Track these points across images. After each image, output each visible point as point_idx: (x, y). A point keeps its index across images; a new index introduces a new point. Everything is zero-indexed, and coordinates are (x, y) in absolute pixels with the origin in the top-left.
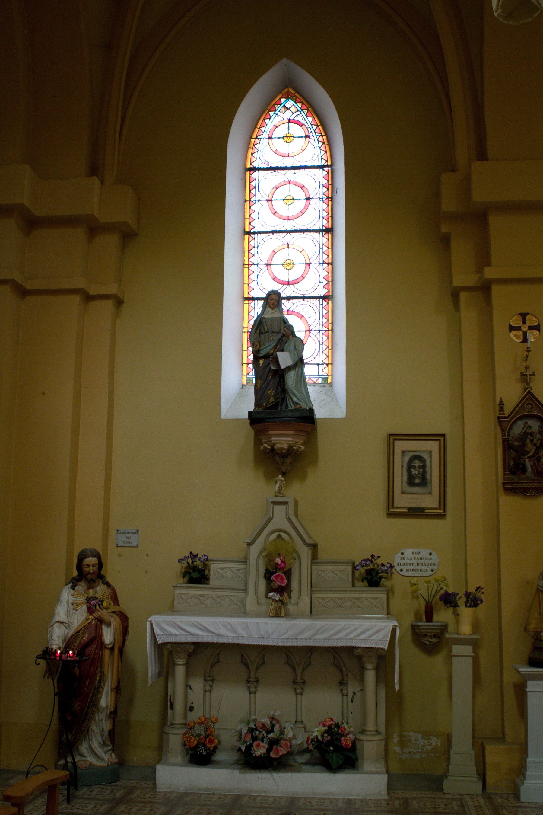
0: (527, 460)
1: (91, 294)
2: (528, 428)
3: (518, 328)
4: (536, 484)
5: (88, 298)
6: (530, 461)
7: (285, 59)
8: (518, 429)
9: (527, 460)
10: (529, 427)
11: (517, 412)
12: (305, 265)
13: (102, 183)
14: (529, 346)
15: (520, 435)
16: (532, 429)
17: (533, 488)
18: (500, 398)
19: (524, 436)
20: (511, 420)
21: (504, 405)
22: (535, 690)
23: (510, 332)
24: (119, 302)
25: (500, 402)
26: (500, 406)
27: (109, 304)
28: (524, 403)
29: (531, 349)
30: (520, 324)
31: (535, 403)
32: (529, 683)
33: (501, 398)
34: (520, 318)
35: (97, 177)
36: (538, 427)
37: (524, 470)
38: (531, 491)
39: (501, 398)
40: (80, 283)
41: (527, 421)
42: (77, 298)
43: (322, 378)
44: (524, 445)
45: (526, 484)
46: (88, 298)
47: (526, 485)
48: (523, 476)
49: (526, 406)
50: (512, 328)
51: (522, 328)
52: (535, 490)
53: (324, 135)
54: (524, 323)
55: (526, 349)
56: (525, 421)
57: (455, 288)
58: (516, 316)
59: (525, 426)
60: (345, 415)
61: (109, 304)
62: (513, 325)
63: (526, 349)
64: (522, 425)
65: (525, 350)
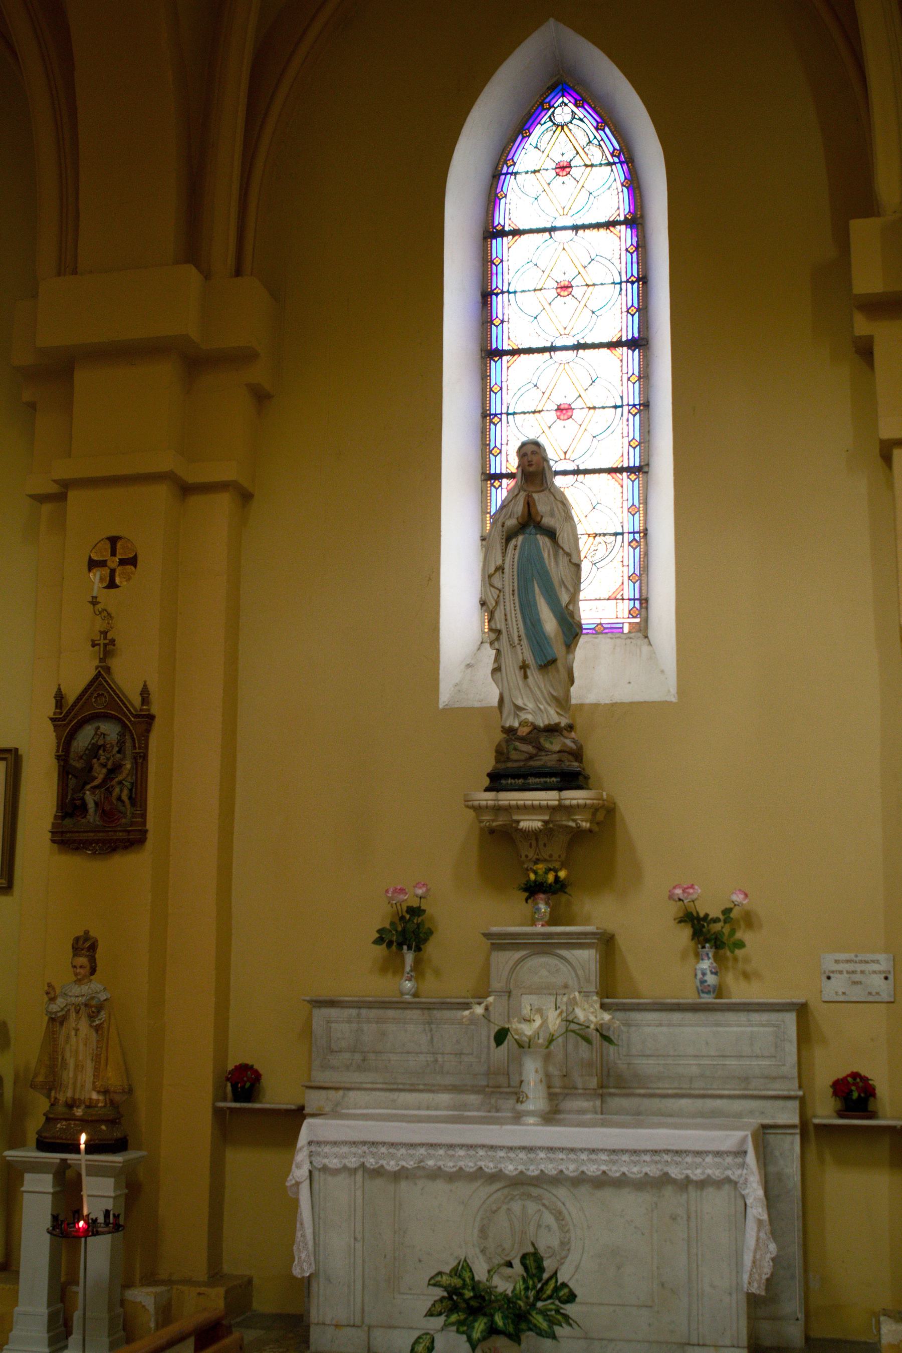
0: (88, 793)
1: (190, 482)
2: (100, 736)
3: (102, 564)
4: (101, 834)
5: (186, 490)
6: (93, 793)
7: (552, 21)
8: (85, 738)
9: (88, 793)
10: (102, 736)
11: (80, 709)
12: (555, 412)
13: (207, 276)
14: (95, 594)
15: (87, 749)
16: (108, 738)
17: (97, 842)
18: (57, 687)
19: (95, 750)
20: (69, 724)
21: (149, 694)
22: (37, 1190)
23: (90, 570)
24: (245, 497)
25: (143, 688)
26: (142, 697)
27: (224, 502)
28: (92, 694)
29: (98, 600)
30: (107, 555)
31: (109, 692)
32: (28, 1177)
33: (145, 682)
34: (108, 546)
35: (197, 267)
36: (117, 734)
37: (84, 808)
38: (95, 846)
39: (145, 682)
40: (165, 462)
41: (100, 724)
42: (162, 492)
43: (630, 623)
44: (91, 768)
45: (85, 834)
46: (186, 490)
47: (84, 836)
48: (83, 820)
49: (96, 698)
50: (93, 564)
51: (109, 563)
52: (100, 845)
53: (617, 163)
54: (113, 554)
55: (90, 599)
56: (96, 725)
57: (882, 442)
58: (102, 542)
59: (96, 734)
60: (673, 690)
61: (224, 502)
62: (96, 558)
63: (90, 599)
64: (93, 732)
65: (89, 602)
